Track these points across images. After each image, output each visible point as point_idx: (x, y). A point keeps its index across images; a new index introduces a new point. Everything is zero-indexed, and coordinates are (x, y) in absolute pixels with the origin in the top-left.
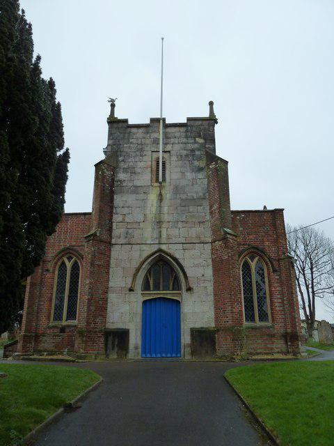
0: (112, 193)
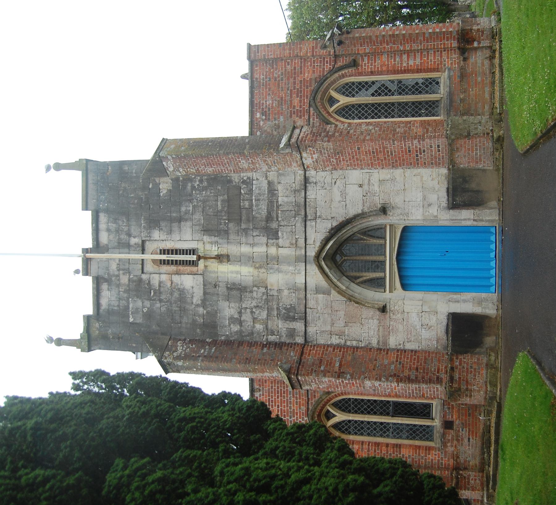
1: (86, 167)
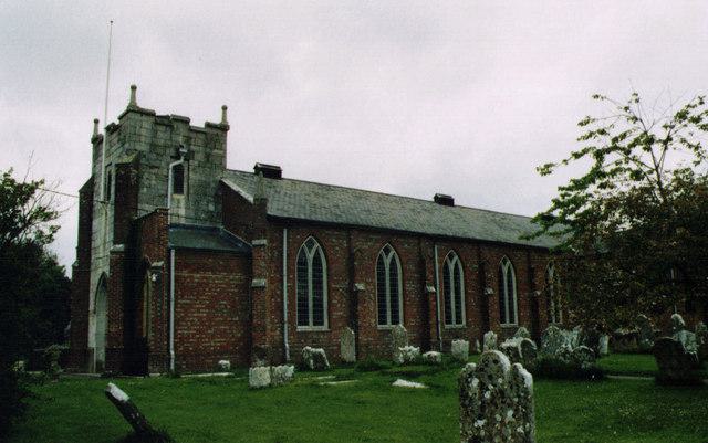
0: (91, 220)
1: (224, 128)
